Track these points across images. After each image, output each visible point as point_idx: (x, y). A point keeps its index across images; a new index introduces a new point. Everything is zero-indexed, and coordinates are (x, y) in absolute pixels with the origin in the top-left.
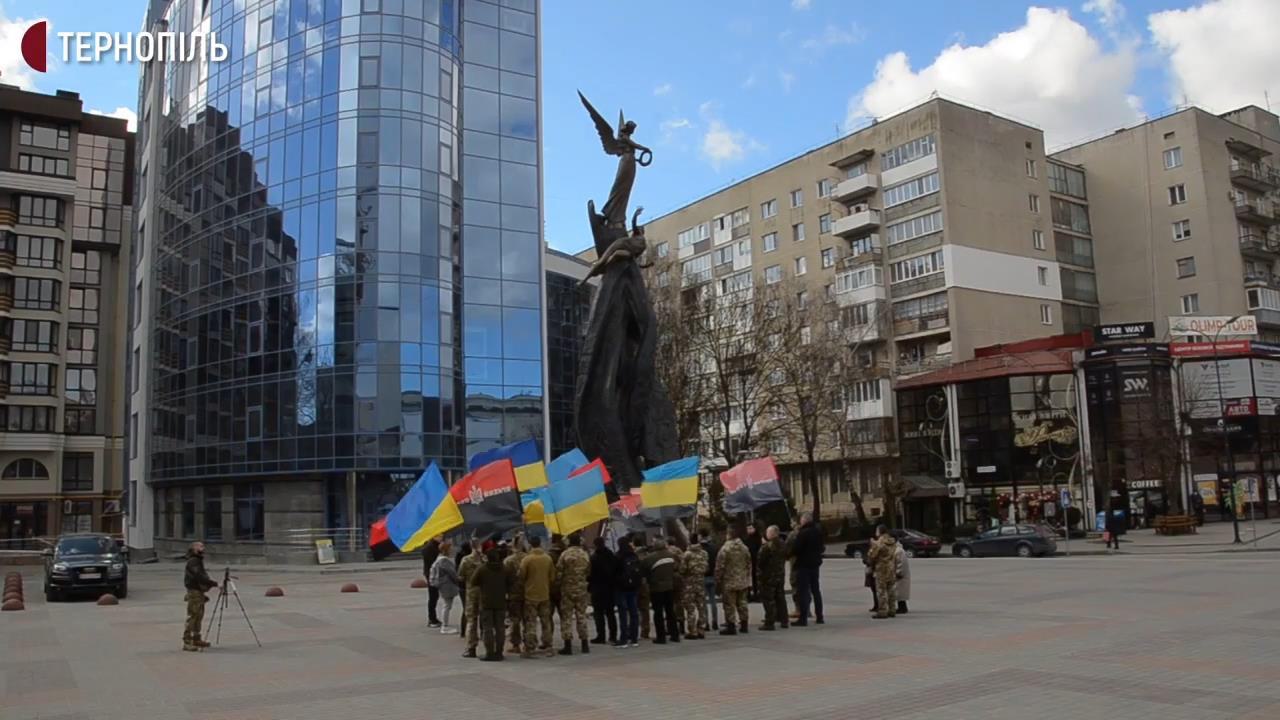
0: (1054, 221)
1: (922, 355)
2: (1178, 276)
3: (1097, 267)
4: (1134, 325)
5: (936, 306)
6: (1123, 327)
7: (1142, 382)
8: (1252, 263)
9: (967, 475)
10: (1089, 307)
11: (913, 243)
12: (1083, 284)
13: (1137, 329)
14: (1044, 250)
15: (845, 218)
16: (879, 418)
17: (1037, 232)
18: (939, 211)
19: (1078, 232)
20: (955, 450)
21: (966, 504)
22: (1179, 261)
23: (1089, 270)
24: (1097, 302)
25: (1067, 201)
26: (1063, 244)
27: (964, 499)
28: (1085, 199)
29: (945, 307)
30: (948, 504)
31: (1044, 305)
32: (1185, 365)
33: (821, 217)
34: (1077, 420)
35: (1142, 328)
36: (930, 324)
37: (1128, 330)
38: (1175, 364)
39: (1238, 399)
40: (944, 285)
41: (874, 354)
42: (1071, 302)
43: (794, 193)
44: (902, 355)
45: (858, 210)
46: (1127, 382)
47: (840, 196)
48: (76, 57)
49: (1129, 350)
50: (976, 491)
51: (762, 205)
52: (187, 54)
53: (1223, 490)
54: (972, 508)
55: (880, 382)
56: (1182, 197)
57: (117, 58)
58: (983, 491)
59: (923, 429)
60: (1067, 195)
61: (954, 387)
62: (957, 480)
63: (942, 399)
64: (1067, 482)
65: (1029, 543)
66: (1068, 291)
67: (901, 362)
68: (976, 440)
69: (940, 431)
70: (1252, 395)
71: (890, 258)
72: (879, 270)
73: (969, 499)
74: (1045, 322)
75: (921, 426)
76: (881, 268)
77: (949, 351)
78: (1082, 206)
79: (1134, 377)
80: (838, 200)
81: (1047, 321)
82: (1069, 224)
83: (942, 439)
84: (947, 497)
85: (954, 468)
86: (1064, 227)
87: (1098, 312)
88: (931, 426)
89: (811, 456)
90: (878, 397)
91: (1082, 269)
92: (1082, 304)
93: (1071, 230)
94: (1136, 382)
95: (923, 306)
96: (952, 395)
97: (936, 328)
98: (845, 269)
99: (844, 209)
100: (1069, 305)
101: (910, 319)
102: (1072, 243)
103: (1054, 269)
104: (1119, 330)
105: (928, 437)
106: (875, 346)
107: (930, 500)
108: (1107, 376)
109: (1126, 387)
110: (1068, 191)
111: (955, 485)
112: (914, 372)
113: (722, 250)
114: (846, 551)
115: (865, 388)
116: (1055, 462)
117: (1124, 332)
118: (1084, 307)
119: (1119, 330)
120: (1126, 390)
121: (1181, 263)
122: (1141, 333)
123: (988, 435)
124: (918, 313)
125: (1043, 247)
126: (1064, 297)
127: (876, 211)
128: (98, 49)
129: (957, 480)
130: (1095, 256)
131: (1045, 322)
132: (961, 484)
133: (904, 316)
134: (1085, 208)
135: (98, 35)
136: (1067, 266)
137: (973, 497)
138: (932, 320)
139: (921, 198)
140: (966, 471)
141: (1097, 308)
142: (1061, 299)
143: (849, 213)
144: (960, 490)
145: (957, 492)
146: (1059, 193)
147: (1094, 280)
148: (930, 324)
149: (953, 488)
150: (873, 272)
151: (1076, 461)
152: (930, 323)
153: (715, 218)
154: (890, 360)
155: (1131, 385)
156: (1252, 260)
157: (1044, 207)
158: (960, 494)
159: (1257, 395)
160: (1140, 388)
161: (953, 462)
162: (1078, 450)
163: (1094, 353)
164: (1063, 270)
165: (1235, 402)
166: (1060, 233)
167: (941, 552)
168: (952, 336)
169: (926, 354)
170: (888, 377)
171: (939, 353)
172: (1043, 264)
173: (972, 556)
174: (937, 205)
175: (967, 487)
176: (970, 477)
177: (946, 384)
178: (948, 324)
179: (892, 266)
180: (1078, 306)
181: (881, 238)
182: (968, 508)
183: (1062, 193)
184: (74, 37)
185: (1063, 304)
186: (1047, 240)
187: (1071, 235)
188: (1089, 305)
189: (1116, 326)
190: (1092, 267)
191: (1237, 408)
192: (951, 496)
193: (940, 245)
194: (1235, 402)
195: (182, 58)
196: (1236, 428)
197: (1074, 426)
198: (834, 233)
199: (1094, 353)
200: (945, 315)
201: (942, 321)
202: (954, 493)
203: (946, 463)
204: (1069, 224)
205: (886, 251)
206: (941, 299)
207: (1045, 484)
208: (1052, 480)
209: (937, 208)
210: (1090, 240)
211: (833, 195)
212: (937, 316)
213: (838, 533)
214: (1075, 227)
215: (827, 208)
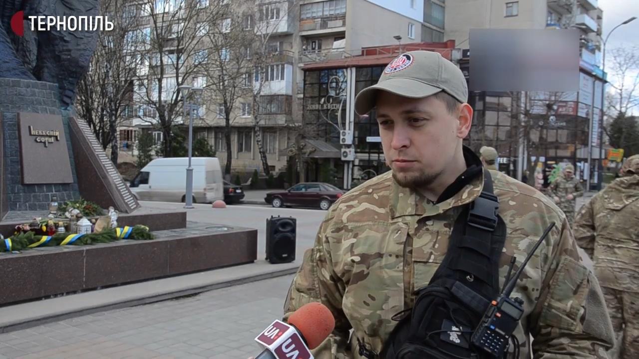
1: (320, 47)
2: (505, 15)
3: (446, 3)
5: (336, 10)
8: (551, 13)
9: (357, 143)
12: (436, 14)
16: (282, 95)
20: (350, 122)
21: (354, 166)
22: (507, 3)
24: (444, 29)
27: (353, 162)
30: (339, 164)
31: (411, 22)
36: (330, 24)
39: (566, 102)
41: (281, 43)
42: (428, 25)
44: (304, 47)
50: (365, 156)
52: (93, 26)
53: (547, 169)
54: (359, 170)
55: (286, 65)
58: (379, 157)
59: (324, 102)
61: (354, 70)
62: (349, 146)
65: (329, 198)
67: (303, 52)
68: (367, 116)
69: (338, 106)
70: (576, 100)
73: (357, 163)
74: (410, 36)
75: (323, 100)
83: (339, 114)
84: (340, 159)
85: (348, 135)
87: (443, 36)
88: (331, 100)
89: (227, 119)
90: (282, 78)
92: (435, 28)
97: (335, 27)
100: (425, 26)
101: (314, 18)
105: (328, 110)
106: (286, 36)
107: (327, 160)
111: (347, 150)
112: (316, 59)
114: (266, 199)
115: (272, 70)
124: (320, 14)
128: (49, 24)
129: (349, 146)
131: (410, 36)
132: (352, 150)
133: (309, 16)
137: (360, 161)
138: (331, 20)
140: (356, 139)
144: (350, 154)
145: (349, 156)
147: (444, 12)
149: (345, 152)
152: (329, 22)
154: (295, 49)
156: (552, 11)
158: (350, 157)
159: (580, 100)
161: (347, 131)
165: (564, 104)
167: (244, 199)
168: (347, 35)
169: (323, 47)
170: (292, 64)
171: (334, 47)
173: (281, 206)
175: (356, 152)
177: (346, 67)
178: (344, 24)
180: (432, 29)
182: (356, 168)
188: (438, 30)
191: (564, 109)
192: (343, 159)
194: (564, 104)
195: (91, 29)
196: (561, 124)
200: (343, 17)
201: (340, 22)
202: (346, 156)
203: (341, 132)
212: (336, 18)
213: (249, 183)
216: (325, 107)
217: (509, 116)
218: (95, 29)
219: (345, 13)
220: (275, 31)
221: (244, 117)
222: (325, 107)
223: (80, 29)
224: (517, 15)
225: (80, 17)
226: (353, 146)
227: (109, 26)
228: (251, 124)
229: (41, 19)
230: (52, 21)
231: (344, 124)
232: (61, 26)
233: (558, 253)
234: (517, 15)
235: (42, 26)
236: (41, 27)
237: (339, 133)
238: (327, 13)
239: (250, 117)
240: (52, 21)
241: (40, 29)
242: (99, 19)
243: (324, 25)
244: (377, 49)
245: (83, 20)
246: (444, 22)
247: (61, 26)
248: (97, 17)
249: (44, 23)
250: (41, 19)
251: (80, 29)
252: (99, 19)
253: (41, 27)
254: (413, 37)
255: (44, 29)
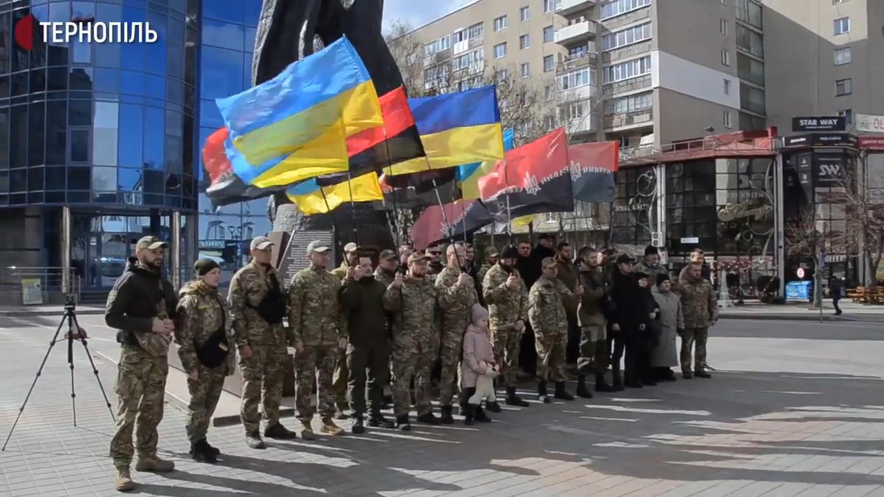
0: (737, 44)
2: (836, 94)
4: (828, 118)
6: (818, 119)
7: (835, 168)
9: (670, 245)
10: (759, 118)
11: (625, 49)
12: (755, 99)
13: (830, 122)
14: (728, 66)
15: (565, 28)
17: (724, 51)
18: (650, 22)
19: (754, 55)
22: (837, 81)
23: (761, 88)
24: (765, 114)
25: (748, 28)
26: (743, 63)
28: (761, 29)
29: (651, 104)
31: (727, 110)
32: (870, 156)
33: (545, 29)
34: (773, 201)
35: (835, 121)
37: (823, 122)
38: (862, 155)
40: (651, 85)
43: (522, 10)
45: (578, 21)
46: (822, 167)
47: (563, 9)
48: (52, 39)
49: (826, 139)
51: (496, 20)
52: (129, 37)
56: (846, 29)
57: (81, 40)
59: (633, 203)
60: (748, 23)
63: (651, 177)
64: (761, 254)
66: (745, 102)
71: (604, 63)
72: (594, 73)
74: (726, 125)
75: (631, 200)
76: (595, 71)
77: (651, 142)
78: (759, 34)
79: (828, 163)
80: (560, 13)
81: (728, 124)
82: (748, 48)
86: (744, 49)
88: (640, 201)
91: (755, 86)
92: (754, 114)
93: (750, 53)
94: (830, 168)
95: (637, 102)
96: (660, 174)
98: (564, 71)
99: (565, 21)
100: (744, 113)
102: (749, 64)
103: (735, 83)
104: (815, 122)
105: (637, 211)
108: (804, 162)
109: (821, 171)
110: (749, 21)
113: (460, 57)
116: (752, 237)
117: (819, 124)
118: (755, 116)
119: (815, 122)
120: (821, 174)
121: (839, 83)
122: (833, 126)
123: (694, 212)
125: (728, 63)
126: (742, 107)
127: (594, 22)
128: (68, 34)
130: (765, 77)
131: (726, 125)
134: (761, 36)
135: (68, 24)
136: (745, 82)
138: (637, 115)
139: (634, 11)
140: (670, 241)
141: (764, 119)
142: (739, 108)
143: (570, 24)
146: (743, 21)
148: (636, 118)
150: (589, 72)
151: (770, 236)
152: (635, 117)
153: (456, 32)
155: (825, 169)
157: (730, 31)
160: (833, 173)
162: (773, 226)
163: (792, 141)
164: (742, 84)
166: (741, 54)
172: (728, 77)
174: (647, 17)
175: (670, 255)
176: (674, 247)
177: (655, 165)
178: (651, 118)
179: (604, 68)
181: (596, 45)
183: (745, 22)
184: (51, 26)
185: (740, 112)
186: (731, 59)
187: (749, 57)
188: (759, 116)
189: (812, 118)
190: (764, 86)
193: (649, 51)
195: (126, 40)
197: (770, 205)
198: (556, 41)
199: (792, 141)
200: (650, 111)
201: (647, 116)
203: (653, 233)
204: (748, 48)
205: (600, 58)
206: (649, 97)
207: (742, 255)
208: (748, 252)
209: (648, 20)
210: (763, 63)
211: (557, 9)
214: (753, 50)
215: (551, 21)
216: (634, 208)
217: (842, 210)
218: (131, 41)
219: (652, 106)
220: (578, 130)
221: (548, 222)
222: (634, 208)
223: (111, 40)
224: (850, 94)
225: (111, 24)
226: (666, 249)
227: (151, 36)
228: (557, 230)
229: (57, 26)
230: (71, 28)
231: (655, 225)
232: (85, 36)
233: (81, 433)
234: (850, 94)
235: (58, 36)
236: (57, 38)
237: (650, 236)
238: (632, 108)
239: (554, 222)
240: (71, 28)
241: (55, 40)
242: (137, 27)
243: (630, 120)
244: (688, 142)
245: (115, 27)
246: (765, 109)
247: (85, 36)
248: (134, 24)
249: (61, 32)
250: (57, 26)
251: (111, 40)
252: (137, 27)
253: (57, 38)
254: (730, 126)
255: (61, 41)
